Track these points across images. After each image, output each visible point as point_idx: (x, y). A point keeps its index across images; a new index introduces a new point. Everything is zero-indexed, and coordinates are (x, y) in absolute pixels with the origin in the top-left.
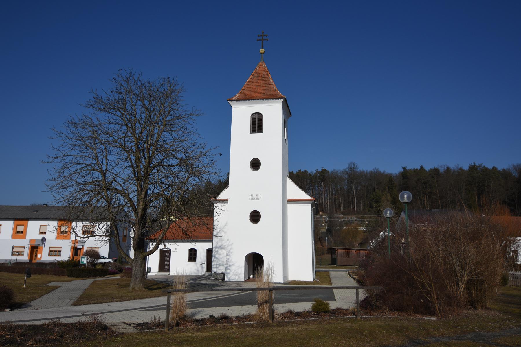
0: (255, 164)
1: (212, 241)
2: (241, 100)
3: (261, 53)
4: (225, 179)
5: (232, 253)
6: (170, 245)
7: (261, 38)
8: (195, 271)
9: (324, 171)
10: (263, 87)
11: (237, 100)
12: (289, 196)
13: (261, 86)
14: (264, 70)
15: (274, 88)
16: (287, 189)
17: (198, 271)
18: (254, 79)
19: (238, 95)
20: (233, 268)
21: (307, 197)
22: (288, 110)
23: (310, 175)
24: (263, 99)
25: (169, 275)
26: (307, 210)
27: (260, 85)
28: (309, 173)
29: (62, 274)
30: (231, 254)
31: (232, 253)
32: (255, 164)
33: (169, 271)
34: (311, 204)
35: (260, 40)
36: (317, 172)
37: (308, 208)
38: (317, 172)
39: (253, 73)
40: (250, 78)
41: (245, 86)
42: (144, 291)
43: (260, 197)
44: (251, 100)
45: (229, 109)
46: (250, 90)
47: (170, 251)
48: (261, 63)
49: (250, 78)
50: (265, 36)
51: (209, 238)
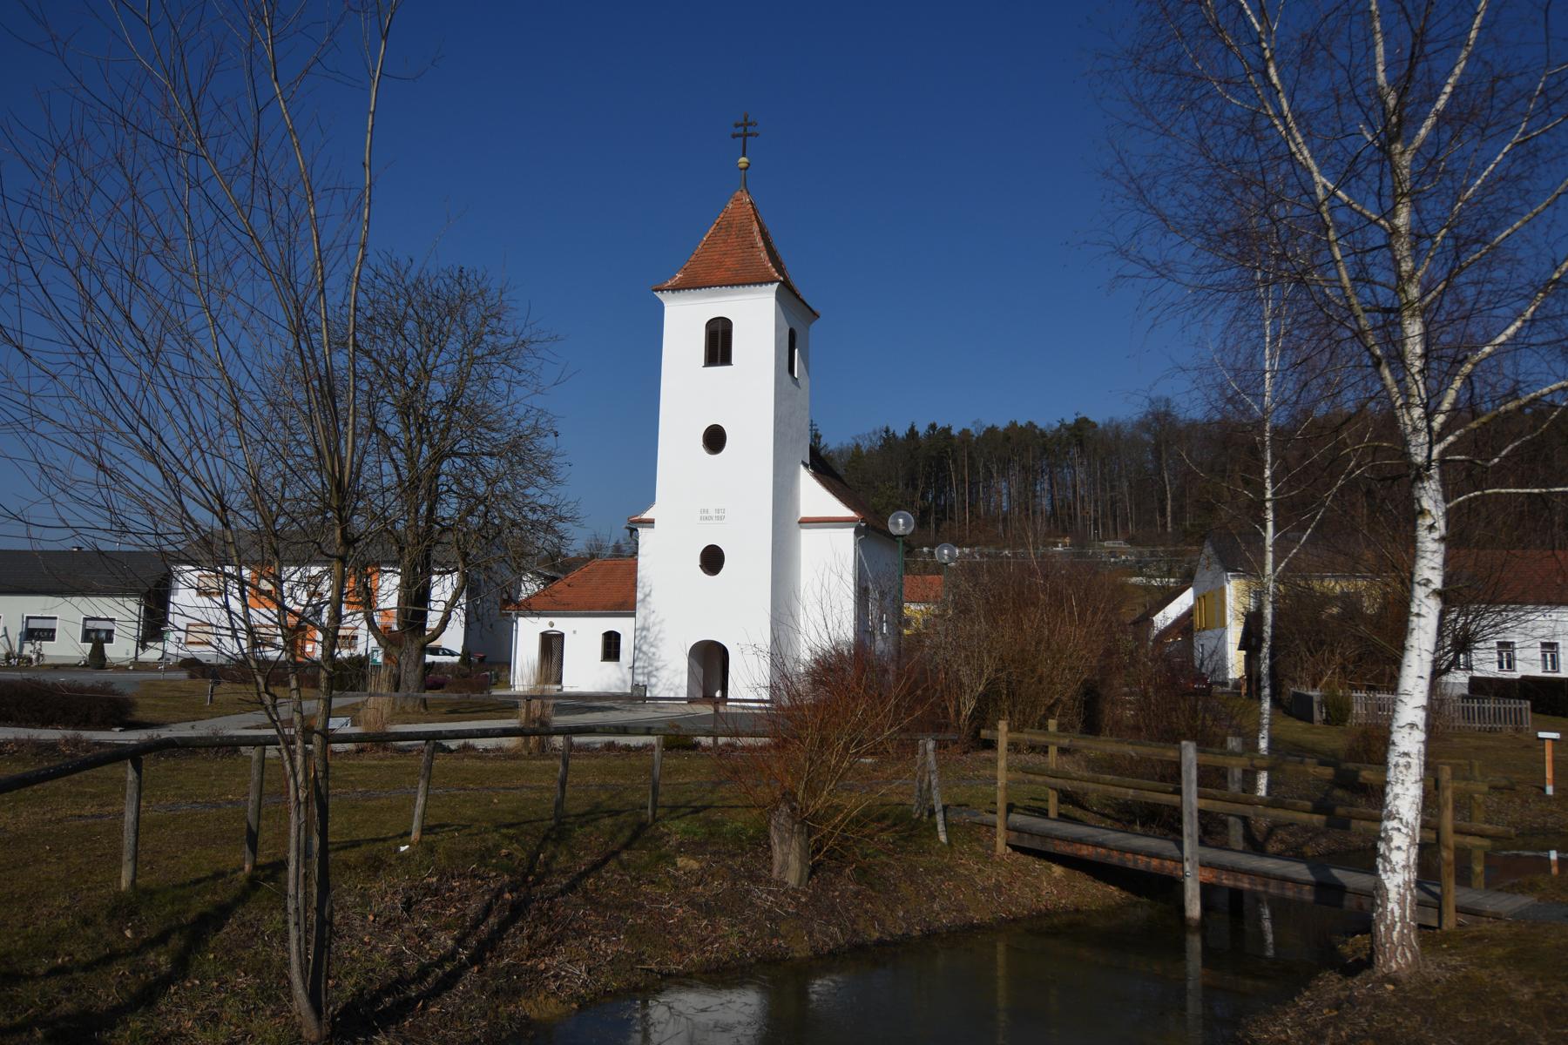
0: (715, 439)
1: (633, 615)
2: (684, 289)
3: (741, 169)
5: (661, 640)
6: (561, 624)
7: (740, 130)
8: (618, 683)
9: (1082, 424)
12: (806, 511)
16: (798, 500)
17: (624, 682)
19: (679, 276)
20: (663, 674)
21: (848, 513)
22: (803, 305)
23: (1043, 434)
24: (732, 285)
25: (558, 690)
26: (844, 541)
28: (1041, 430)
29: (635, 728)
30: (660, 644)
31: (661, 640)
32: (715, 439)
33: (559, 681)
34: (853, 530)
35: (738, 136)
36: (1063, 425)
37: (847, 537)
38: (1063, 425)
40: (710, 232)
41: (696, 252)
42: (422, 714)
44: (705, 287)
45: (659, 309)
47: (561, 636)
48: (739, 193)
49: (710, 232)
50: (750, 124)
51: (626, 606)
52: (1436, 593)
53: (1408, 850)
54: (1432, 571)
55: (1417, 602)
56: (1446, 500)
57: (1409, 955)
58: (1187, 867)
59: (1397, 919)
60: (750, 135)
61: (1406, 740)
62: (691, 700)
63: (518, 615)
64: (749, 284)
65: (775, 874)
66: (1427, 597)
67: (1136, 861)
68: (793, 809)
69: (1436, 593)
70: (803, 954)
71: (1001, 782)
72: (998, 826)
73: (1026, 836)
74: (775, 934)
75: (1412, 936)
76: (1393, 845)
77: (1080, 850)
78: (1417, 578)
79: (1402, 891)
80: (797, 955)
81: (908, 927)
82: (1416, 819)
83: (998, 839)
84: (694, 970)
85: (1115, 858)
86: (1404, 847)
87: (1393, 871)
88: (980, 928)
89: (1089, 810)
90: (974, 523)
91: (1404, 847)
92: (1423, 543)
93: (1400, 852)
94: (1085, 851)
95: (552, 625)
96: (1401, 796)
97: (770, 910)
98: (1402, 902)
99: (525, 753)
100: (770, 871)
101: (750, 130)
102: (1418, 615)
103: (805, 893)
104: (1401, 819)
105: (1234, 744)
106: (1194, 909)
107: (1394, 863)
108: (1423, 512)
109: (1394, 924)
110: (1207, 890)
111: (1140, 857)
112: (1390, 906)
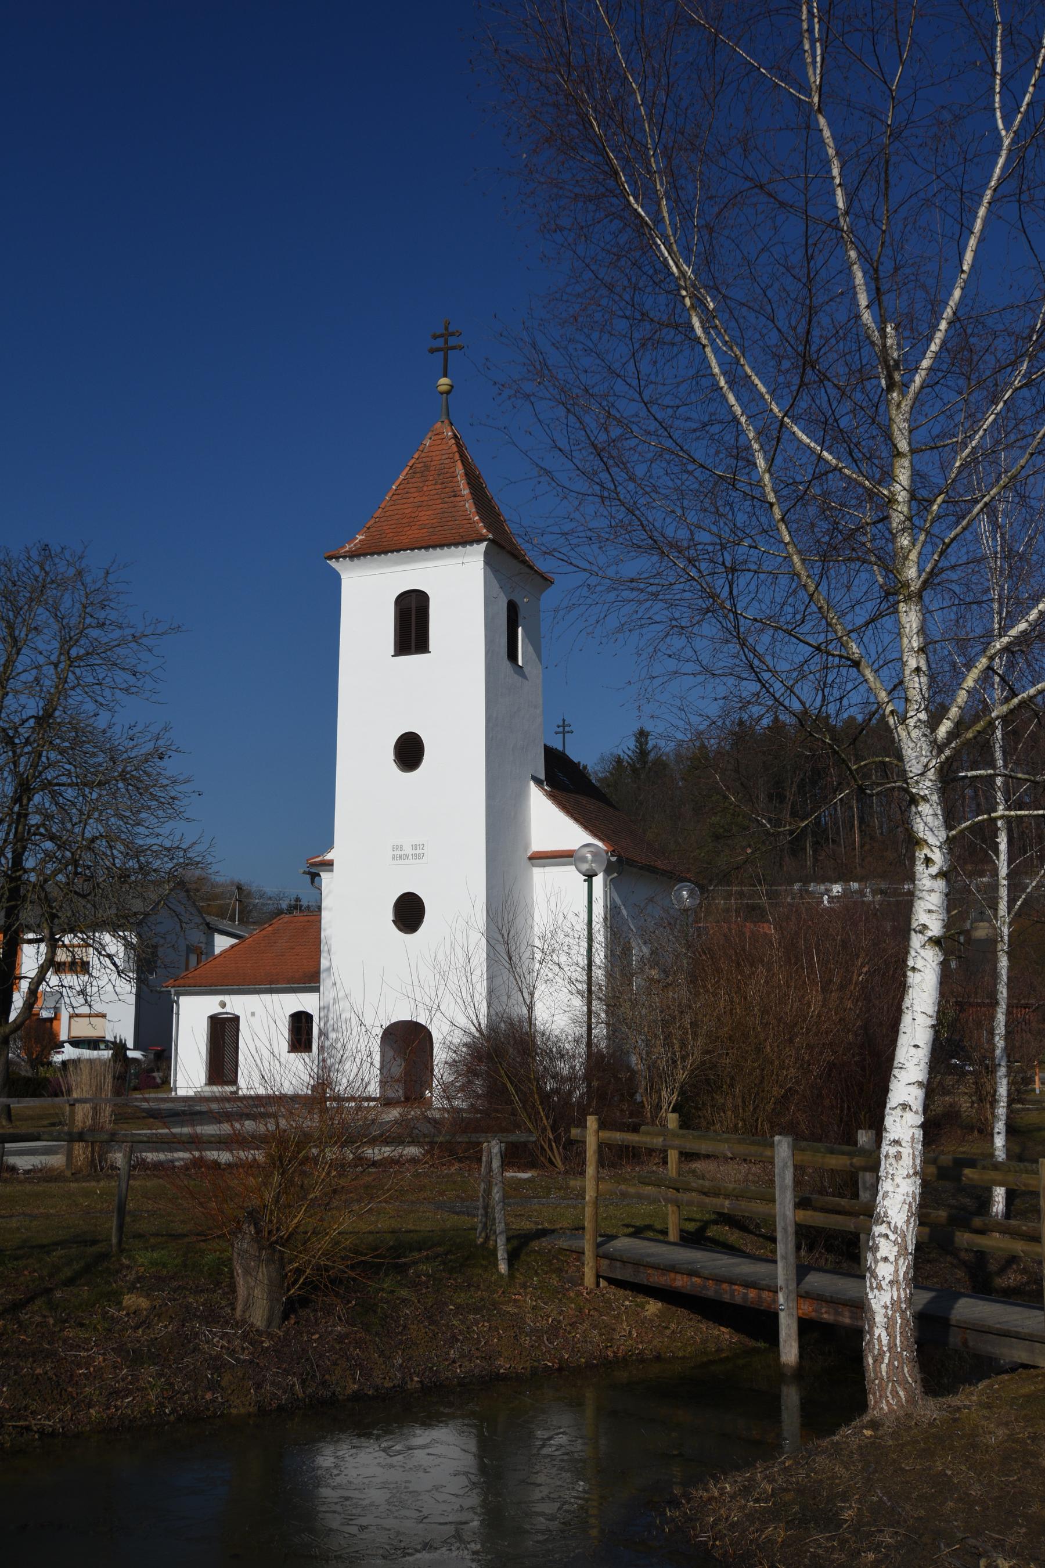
1: (317, 990)
2: (365, 555)
3: (442, 393)
4: (630, 753)
6: (237, 1004)
7: (440, 343)
10: (434, 507)
11: (354, 555)
12: (539, 843)
13: (430, 503)
14: (444, 447)
15: (467, 505)
18: (413, 480)
19: (360, 537)
24: (427, 548)
25: (232, 1093)
27: (426, 498)
33: (234, 1082)
39: (413, 461)
41: (382, 506)
43: (421, 852)
44: (392, 552)
45: (335, 582)
46: (397, 517)
47: (236, 1019)
48: (438, 425)
50: (452, 334)
52: (936, 942)
53: (896, 1260)
54: (929, 915)
55: (913, 953)
56: (949, 827)
57: (902, 1393)
58: (781, 1298)
59: (885, 1349)
60: (453, 348)
61: (898, 1125)
62: (387, 1102)
63: (178, 994)
64: (434, 547)
65: (238, 1313)
66: (923, 946)
67: (732, 1292)
68: (258, 1231)
69: (936, 942)
70: (242, 1411)
71: (590, 1195)
72: (587, 1253)
73: (618, 1264)
74: (213, 1386)
75: (906, 1370)
76: (879, 1256)
77: (675, 1279)
78: (914, 925)
79: (890, 1313)
80: (234, 1411)
81: (403, 1378)
82: (907, 1222)
83: (586, 1270)
84: (88, 1428)
85: (711, 1290)
86: (892, 1258)
87: (880, 1288)
88: (504, 1378)
89: (750, 1232)
90: (867, 847)
91: (892, 1258)
92: (920, 880)
93: (887, 1264)
94: (680, 1282)
95: (223, 1005)
96: (890, 1194)
97: (218, 1357)
98: (889, 1327)
99: (68, 1174)
100: (234, 1309)
101: (453, 341)
102: (914, 969)
103: (270, 1336)
104: (889, 1223)
105: (864, 1139)
106: (789, 1352)
107: (880, 1278)
108: (920, 842)
109: (882, 1354)
110: (805, 1327)
111: (736, 1287)
112: (877, 1332)
